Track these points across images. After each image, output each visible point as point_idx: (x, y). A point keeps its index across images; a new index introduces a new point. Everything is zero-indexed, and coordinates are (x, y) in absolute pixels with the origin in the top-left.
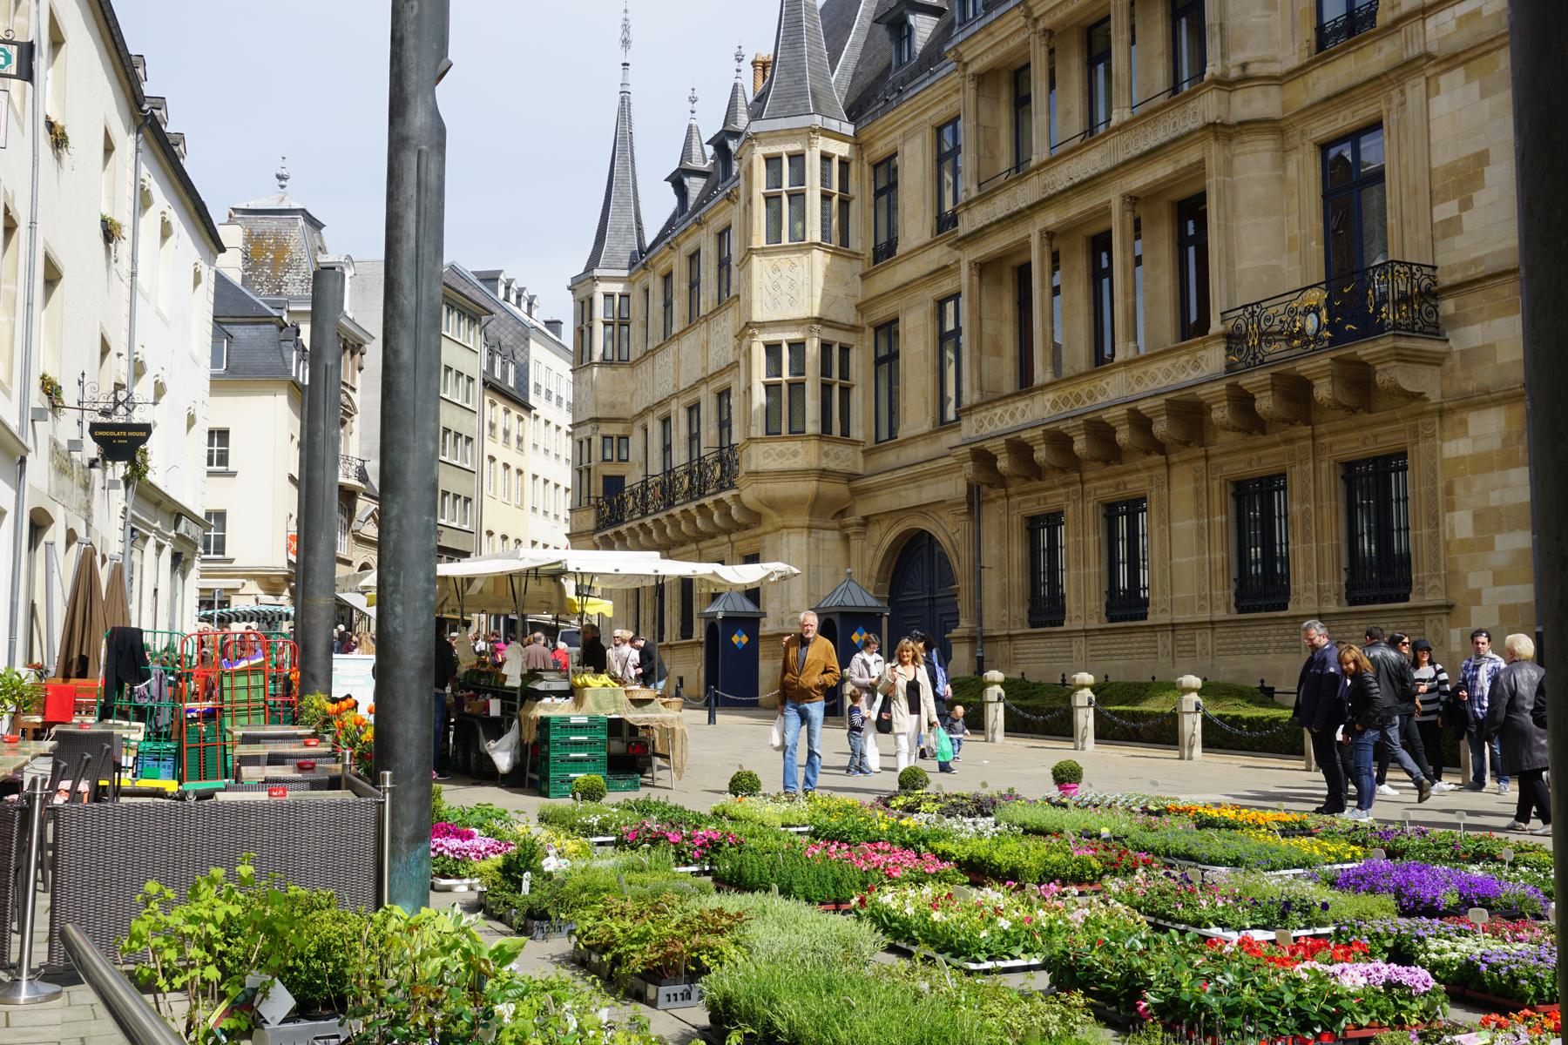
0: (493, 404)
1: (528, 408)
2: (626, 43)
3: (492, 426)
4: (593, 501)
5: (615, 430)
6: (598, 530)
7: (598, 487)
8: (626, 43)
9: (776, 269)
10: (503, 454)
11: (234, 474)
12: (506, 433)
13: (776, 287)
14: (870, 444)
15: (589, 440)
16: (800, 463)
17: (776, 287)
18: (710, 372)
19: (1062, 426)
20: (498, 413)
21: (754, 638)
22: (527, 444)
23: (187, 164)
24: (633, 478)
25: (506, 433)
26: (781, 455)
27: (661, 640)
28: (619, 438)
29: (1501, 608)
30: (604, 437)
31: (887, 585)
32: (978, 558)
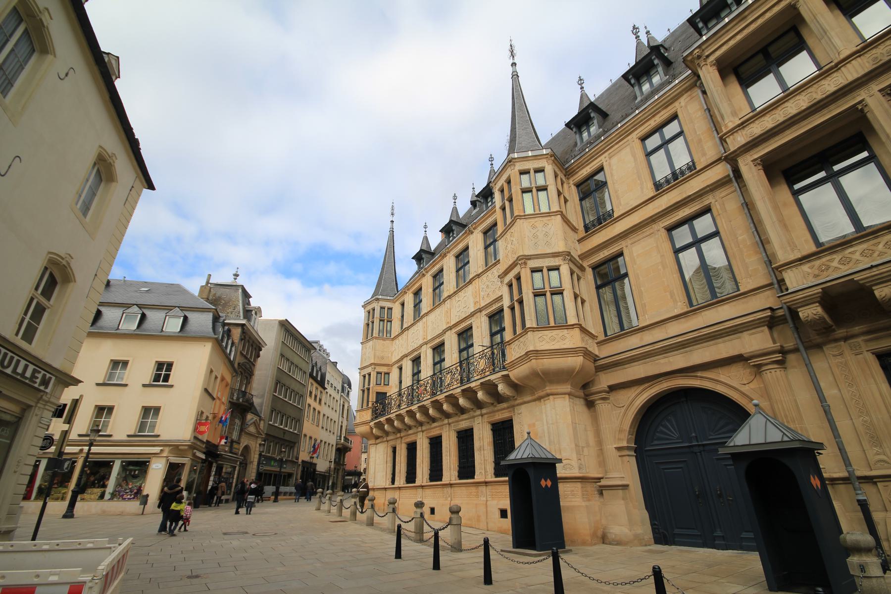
0: (312, 384)
1: (325, 389)
2: (392, 214)
3: (311, 393)
4: (370, 405)
5: (384, 369)
6: (372, 420)
7: (373, 398)
8: (392, 214)
9: (533, 227)
10: (314, 404)
11: (172, 386)
12: (316, 396)
13: (535, 236)
14: (602, 337)
15: (369, 375)
16: (568, 344)
17: (535, 236)
18: (453, 323)
19: (857, 277)
20: (312, 387)
21: (555, 480)
22: (323, 402)
23: (118, 84)
24: (392, 390)
25: (316, 396)
26: (553, 339)
27: (393, 482)
28: (385, 374)
29: (807, 453)
30: (378, 373)
31: (634, 437)
32: (822, 399)
